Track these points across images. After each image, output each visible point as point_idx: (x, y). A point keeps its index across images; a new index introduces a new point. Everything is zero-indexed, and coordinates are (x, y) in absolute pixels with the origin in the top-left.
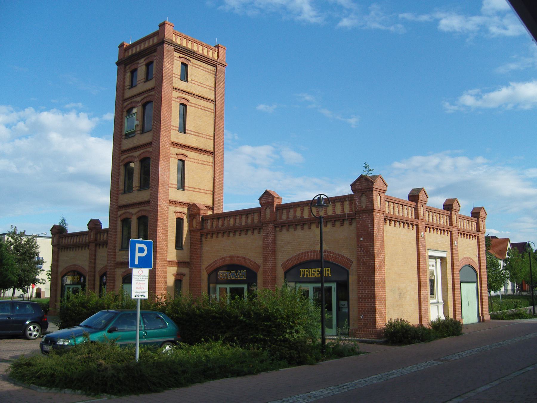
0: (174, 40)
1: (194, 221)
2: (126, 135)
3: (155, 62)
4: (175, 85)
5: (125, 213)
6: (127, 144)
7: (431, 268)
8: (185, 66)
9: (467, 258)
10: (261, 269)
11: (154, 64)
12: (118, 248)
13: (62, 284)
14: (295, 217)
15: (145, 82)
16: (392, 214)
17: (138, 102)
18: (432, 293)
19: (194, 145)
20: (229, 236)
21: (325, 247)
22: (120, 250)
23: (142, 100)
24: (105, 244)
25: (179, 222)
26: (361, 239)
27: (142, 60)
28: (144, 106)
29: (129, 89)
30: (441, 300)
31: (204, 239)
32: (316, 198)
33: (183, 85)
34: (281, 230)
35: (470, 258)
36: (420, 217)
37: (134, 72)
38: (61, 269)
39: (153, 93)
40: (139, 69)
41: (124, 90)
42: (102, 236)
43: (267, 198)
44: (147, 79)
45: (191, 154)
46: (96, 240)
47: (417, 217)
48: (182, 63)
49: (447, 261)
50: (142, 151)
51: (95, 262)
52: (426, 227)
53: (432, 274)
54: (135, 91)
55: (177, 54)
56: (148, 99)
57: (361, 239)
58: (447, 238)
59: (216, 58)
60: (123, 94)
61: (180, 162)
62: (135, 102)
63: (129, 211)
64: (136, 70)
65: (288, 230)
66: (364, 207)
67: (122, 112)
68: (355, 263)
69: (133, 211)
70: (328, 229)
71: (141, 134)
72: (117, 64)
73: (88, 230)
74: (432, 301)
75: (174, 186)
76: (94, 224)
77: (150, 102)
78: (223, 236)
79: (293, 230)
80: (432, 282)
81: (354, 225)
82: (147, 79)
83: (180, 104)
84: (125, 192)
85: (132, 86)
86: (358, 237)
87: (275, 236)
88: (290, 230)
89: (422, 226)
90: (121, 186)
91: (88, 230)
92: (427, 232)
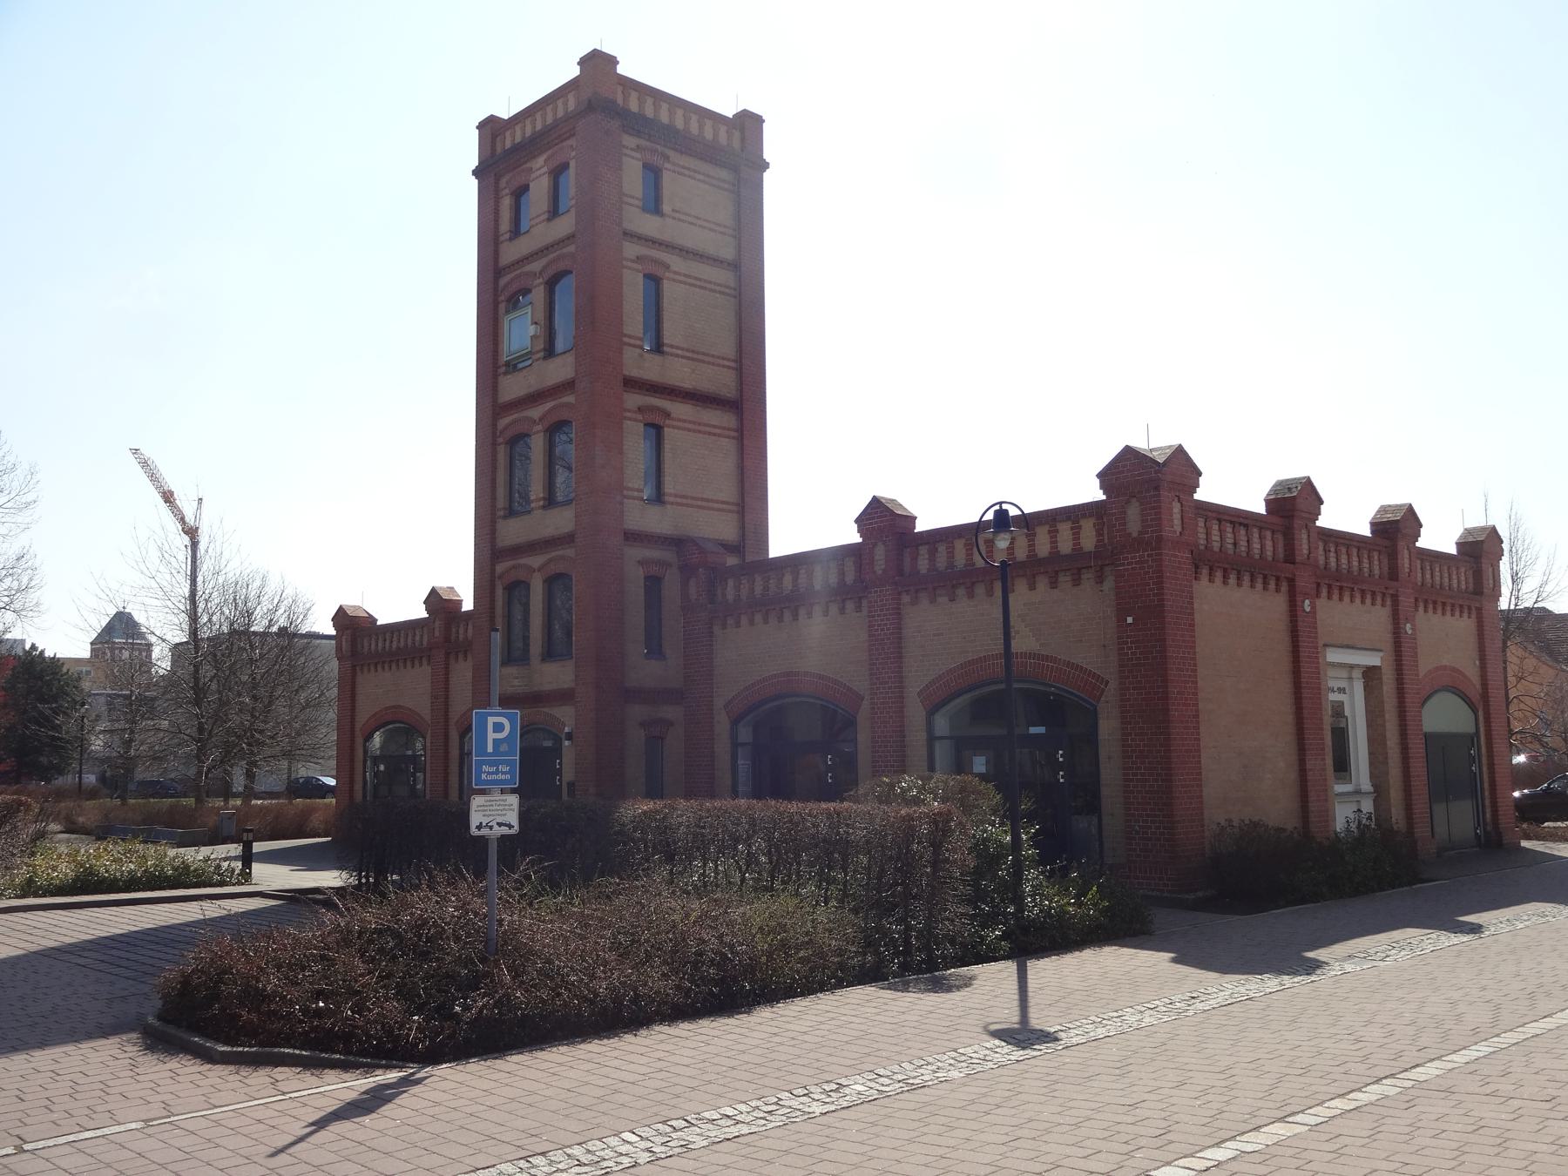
0: (620, 101)
1: (692, 583)
2: (507, 364)
3: (572, 164)
4: (633, 371)
5: (514, 567)
6: (513, 387)
7: (1333, 697)
8: (653, 173)
9: (1445, 668)
10: (866, 704)
11: (572, 171)
12: (496, 658)
13: (365, 752)
14: (951, 565)
15: (549, 220)
16: (1231, 552)
17: (534, 275)
18: (1342, 766)
19: (688, 384)
20: (780, 619)
21: (1017, 645)
22: (504, 663)
23: (545, 268)
24: (464, 649)
25: (653, 584)
26: (1130, 620)
27: (541, 160)
28: (551, 284)
29: (511, 239)
30: (1366, 785)
31: (717, 629)
32: (990, 516)
33: (649, 225)
34: (915, 602)
35: (1454, 670)
36: (1298, 559)
37: (521, 192)
38: (362, 717)
39: (571, 249)
40: (532, 185)
41: (497, 242)
42: (461, 631)
43: (881, 519)
44: (554, 212)
45: (680, 409)
46: (447, 639)
47: (1290, 558)
48: (646, 166)
49: (1385, 678)
50: (549, 405)
51: (447, 697)
52: (1318, 585)
53: (1338, 710)
54: (522, 247)
55: (630, 141)
56: (561, 266)
57: (1130, 620)
58: (1275, 604)
59: (736, 144)
60: (496, 253)
61: (652, 431)
62: (527, 274)
63: (522, 561)
64: (525, 189)
65: (933, 601)
66: (1135, 535)
67: (496, 304)
68: (1113, 685)
69: (536, 561)
70: (1021, 596)
71: (545, 358)
72: (476, 173)
73: (425, 615)
74: (1340, 788)
75: (636, 202)
76: (438, 602)
77: (567, 272)
78: (766, 621)
79: (945, 599)
80: (1341, 736)
81: (1109, 584)
82: (554, 212)
83: (645, 276)
84: (511, 513)
85: (516, 232)
86: (1121, 619)
87: (898, 614)
88: (940, 599)
89: (1304, 581)
90: (501, 502)
91: (425, 615)
92: (1322, 603)
